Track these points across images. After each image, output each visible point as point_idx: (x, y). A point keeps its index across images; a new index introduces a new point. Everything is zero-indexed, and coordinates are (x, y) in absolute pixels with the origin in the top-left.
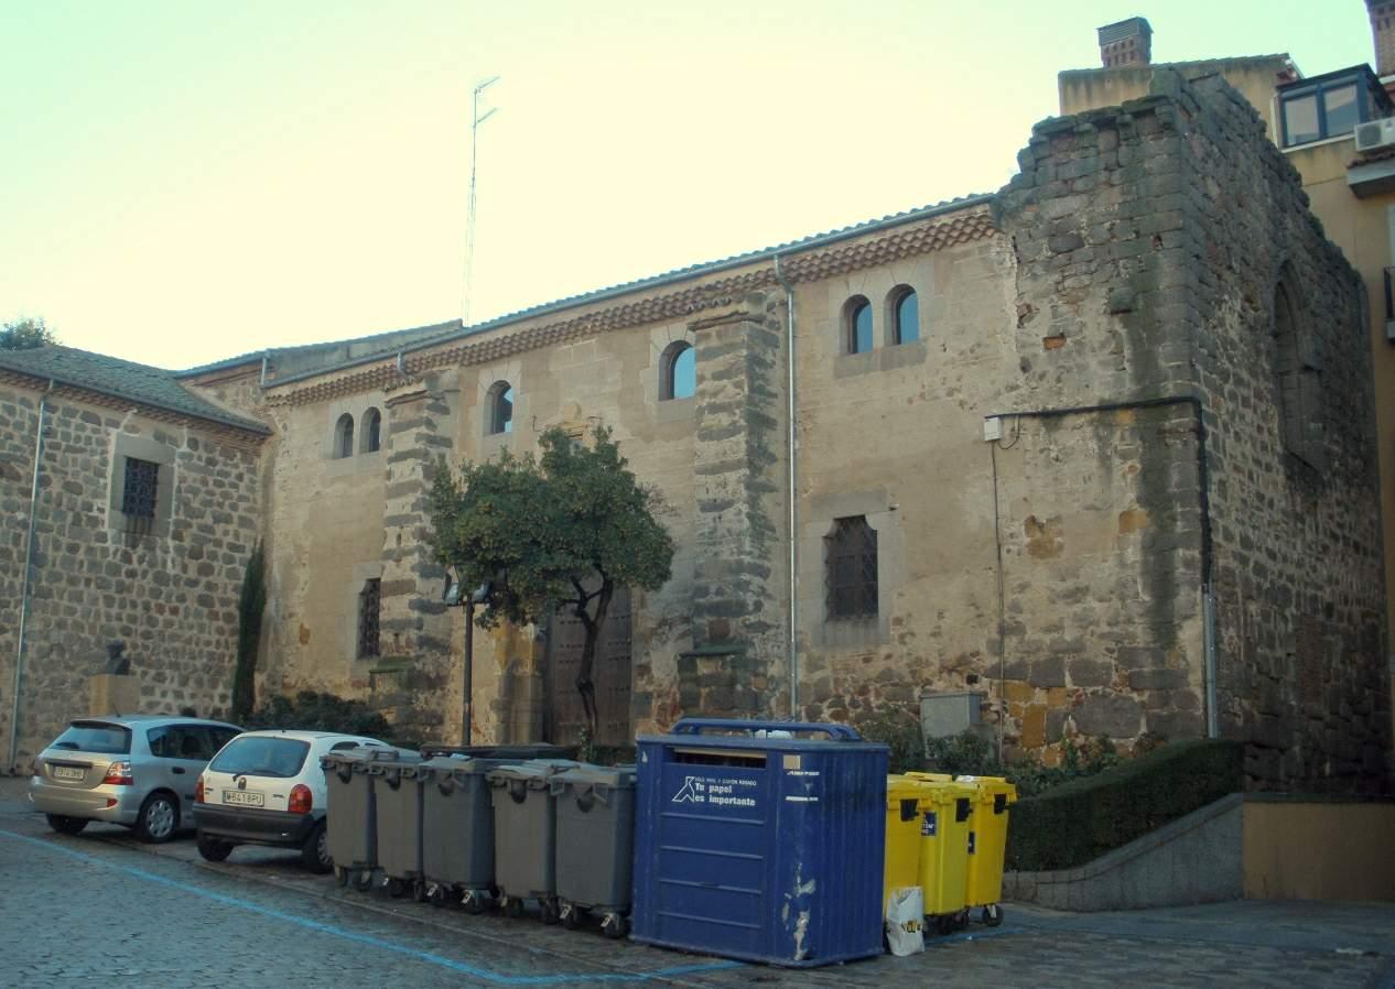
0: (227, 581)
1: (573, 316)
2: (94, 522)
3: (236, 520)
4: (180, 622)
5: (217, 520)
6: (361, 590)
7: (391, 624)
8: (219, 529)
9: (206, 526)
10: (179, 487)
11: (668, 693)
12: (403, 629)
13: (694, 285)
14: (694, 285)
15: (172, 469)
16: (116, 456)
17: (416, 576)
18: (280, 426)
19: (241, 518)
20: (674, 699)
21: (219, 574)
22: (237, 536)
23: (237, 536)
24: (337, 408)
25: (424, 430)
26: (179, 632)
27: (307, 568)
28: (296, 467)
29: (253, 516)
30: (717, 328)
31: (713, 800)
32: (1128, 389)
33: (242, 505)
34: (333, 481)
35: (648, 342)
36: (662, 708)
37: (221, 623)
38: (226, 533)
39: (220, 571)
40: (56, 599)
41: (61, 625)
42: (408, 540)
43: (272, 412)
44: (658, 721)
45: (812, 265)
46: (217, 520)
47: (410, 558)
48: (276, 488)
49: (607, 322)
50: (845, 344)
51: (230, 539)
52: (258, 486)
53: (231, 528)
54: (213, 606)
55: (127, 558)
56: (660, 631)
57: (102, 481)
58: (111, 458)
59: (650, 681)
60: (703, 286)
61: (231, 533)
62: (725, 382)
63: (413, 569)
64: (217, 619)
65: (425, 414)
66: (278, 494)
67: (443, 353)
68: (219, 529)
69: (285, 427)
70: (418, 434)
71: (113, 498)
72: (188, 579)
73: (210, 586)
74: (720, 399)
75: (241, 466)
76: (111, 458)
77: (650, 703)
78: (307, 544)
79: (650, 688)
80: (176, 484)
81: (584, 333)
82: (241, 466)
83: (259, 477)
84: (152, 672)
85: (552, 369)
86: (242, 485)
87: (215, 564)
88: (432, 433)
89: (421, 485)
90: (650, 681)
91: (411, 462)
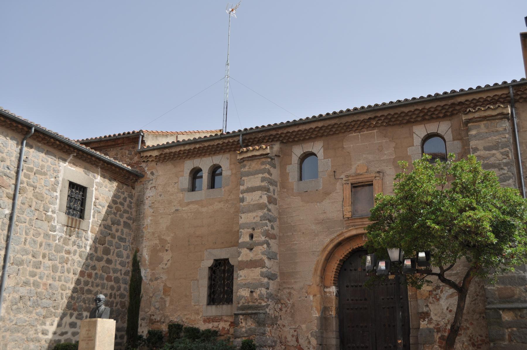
0: (117, 258)
2: (49, 219)
3: (122, 223)
4: (92, 282)
5: (113, 223)
6: (210, 266)
7: (246, 286)
8: (114, 228)
9: (108, 225)
10: (95, 202)
12: (257, 288)
13: (450, 102)
14: (450, 102)
15: (93, 191)
16: (63, 180)
17: (265, 258)
18: (149, 173)
19: (124, 222)
21: (113, 255)
22: (122, 233)
23: (122, 233)
24: (189, 165)
25: (266, 175)
26: (91, 288)
27: (169, 252)
28: (160, 195)
29: (130, 222)
30: (485, 122)
32: (66, 224)
33: (126, 215)
34: (188, 204)
35: (411, 134)
37: (112, 283)
38: (117, 231)
39: (113, 253)
40: (25, 266)
41: (26, 283)
42: (259, 236)
43: (143, 165)
45: (433, 114)
46: (113, 223)
47: (261, 247)
48: (146, 207)
49: (386, 121)
50: (190, 188)
51: (118, 234)
52: (133, 205)
53: (120, 228)
54: (110, 273)
55: (66, 242)
56: (434, 293)
57: (55, 194)
58: (60, 179)
60: (456, 102)
61: (120, 231)
62: (494, 152)
63: (263, 253)
64: (111, 281)
65: (268, 167)
66: (147, 210)
67: (271, 135)
68: (114, 228)
69: (152, 174)
70: (262, 178)
71: (61, 205)
72: (98, 256)
73: (109, 261)
74: (492, 160)
75: (126, 193)
76: (60, 179)
78: (168, 239)
79: (431, 326)
80: (94, 200)
81: (369, 126)
82: (126, 193)
83: (134, 201)
84: (76, 313)
85: (345, 146)
86: (126, 204)
87: (111, 248)
88: (271, 178)
89: (266, 206)
90: (430, 322)
91: (259, 193)
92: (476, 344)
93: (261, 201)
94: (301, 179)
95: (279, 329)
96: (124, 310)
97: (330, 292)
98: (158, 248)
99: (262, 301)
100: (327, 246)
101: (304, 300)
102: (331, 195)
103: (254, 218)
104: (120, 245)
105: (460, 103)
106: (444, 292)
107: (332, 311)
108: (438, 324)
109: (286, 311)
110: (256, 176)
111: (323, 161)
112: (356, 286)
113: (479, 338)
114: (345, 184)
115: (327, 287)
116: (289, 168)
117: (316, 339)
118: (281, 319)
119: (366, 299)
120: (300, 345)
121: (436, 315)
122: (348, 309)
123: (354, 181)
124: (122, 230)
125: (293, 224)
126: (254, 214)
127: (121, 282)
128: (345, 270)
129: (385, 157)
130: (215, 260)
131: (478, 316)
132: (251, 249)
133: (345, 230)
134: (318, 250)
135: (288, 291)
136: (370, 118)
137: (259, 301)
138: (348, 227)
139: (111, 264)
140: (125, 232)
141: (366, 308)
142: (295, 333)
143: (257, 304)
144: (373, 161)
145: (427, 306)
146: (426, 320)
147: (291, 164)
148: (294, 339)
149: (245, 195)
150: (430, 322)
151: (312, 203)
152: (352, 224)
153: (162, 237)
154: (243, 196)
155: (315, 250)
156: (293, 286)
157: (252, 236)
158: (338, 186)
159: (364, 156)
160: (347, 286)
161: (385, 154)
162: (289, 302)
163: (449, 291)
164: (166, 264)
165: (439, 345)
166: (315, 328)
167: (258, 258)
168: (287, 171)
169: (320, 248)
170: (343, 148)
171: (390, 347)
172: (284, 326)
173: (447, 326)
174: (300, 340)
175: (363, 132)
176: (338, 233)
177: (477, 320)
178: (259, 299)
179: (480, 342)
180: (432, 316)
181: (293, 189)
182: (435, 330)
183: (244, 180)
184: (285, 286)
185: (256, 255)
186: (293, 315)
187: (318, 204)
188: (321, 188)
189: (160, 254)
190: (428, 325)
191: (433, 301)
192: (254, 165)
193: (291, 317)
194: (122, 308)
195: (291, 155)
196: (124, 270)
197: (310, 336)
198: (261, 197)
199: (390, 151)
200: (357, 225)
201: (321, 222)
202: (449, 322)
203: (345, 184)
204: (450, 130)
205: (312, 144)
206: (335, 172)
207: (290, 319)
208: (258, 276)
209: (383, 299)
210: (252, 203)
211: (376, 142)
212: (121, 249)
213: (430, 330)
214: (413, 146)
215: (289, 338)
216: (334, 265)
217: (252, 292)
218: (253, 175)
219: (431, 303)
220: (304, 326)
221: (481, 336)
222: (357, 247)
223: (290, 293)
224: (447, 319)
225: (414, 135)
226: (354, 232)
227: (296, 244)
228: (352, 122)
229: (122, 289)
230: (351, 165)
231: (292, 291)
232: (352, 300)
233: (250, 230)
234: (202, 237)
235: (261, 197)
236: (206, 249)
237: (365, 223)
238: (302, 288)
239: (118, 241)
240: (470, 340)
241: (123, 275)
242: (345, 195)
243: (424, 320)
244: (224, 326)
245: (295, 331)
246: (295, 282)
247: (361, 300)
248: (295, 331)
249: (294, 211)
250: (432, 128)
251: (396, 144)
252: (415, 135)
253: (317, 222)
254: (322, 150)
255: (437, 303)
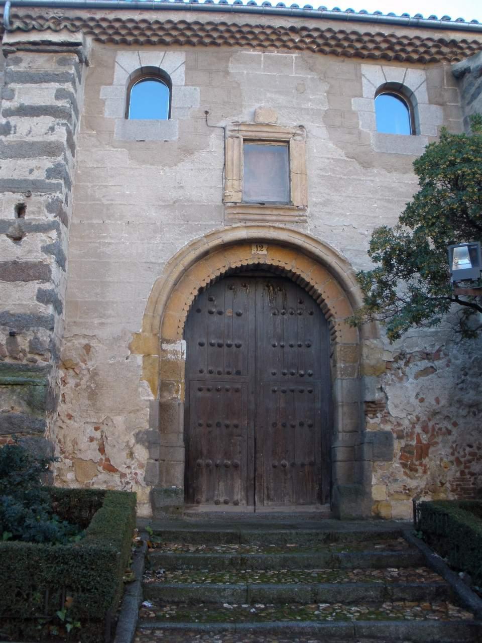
1: (287, 23)
11: (410, 435)
13: (437, 36)
14: (437, 36)
20: (419, 441)
31: (397, 570)
35: (359, 77)
36: (406, 450)
44: (404, 465)
47: (42, 236)
56: (395, 365)
59: (385, 420)
70: (58, 91)
77: (391, 445)
79: (388, 428)
85: (231, 71)
92: (462, 460)
93: (52, 138)
94: (126, 117)
95: (60, 423)
97: (175, 353)
99: (37, 357)
100: (182, 254)
101: (122, 364)
102: (196, 154)
103: (31, 171)
105: (453, 43)
106: (411, 365)
107: (177, 391)
108: (399, 424)
109: (77, 385)
110: (44, 85)
111: (183, 88)
112: (220, 346)
113: (468, 449)
114: (232, 137)
115: (168, 342)
116: (105, 92)
117: (149, 448)
118: (64, 401)
119: (238, 373)
120: (108, 460)
121: (396, 406)
122: (200, 390)
123: (250, 134)
125: (106, 202)
126: (32, 163)
128: (199, 311)
129: (309, 105)
131: (467, 410)
132: (17, 239)
133: (222, 227)
134: (161, 261)
135: (84, 342)
136: (293, 29)
137: (29, 356)
138: (232, 220)
141: (237, 391)
142: (98, 434)
143: (25, 362)
144: (286, 107)
145: (381, 389)
146: (379, 415)
147: (111, 84)
148: (95, 445)
149: (13, 120)
150: (385, 420)
151: (152, 164)
152: (241, 216)
154: (8, 123)
155: (153, 260)
156: (96, 332)
157: (20, 210)
158: (215, 141)
159: (269, 95)
160: (201, 345)
161: (310, 100)
162: (83, 366)
163: (419, 363)
165: (401, 463)
166: (146, 426)
167: (32, 258)
168: (102, 96)
169: (166, 258)
170: (227, 73)
171: (284, 466)
172: (70, 417)
173: (414, 427)
174: (108, 449)
175: (270, 52)
176: (208, 231)
177: (465, 417)
178: (30, 352)
179: (468, 457)
180: (390, 406)
181: (111, 133)
182: (395, 435)
183: (13, 90)
184: (76, 330)
185: (30, 252)
186: (93, 395)
187: (167, 169)
188: (175, 138)
190: (382, 426)
191: (392, 380)
192: (42, 63)
193: (89, 399)
195: (113, 67)
197: (133, 441)
198: (52, 129)
199: (318, 97)
200: (250, 220)
201: (173, 205)
202: (418, 419)
203: (232, 137)
204: (424, 85)
205: (162, 54)
206: (207, 112)
207: (87, 402)
208: (31, 299)
209: (274, 374)
210: (29, 139)
211: (294, 75)
213: (387, 436)
214: (361, 96)
215: (84, 443)
216: (187, 297)
217: (12, 335)
218: (36, 82)
219: (386, 383)
220: (119, 420)
221: (470, 446)
222: (239, 265)
223: (88, 348)
224: (415, 414)
225: (363, 79)
226: (243, 234)
227: (110, 244)
228: (257, 26)
230: (241, 106)
231: (93, 343)
232: (211, 372)
233: (19, 198)
235: (52, 129)
237: (268, 218)
238: (117, 339)
240: (453, 454)
242: (229, 158)
243: (375, 416)
245: (96, 429)
246: (102, 324)
247: (229, 373)
248: (96, 429)
249: (112, 177)
250: (395, 74)
251: (331, 87)
252: (364, 80)
253: (161, 203)
254: (183, 68)
255: (398, 385)
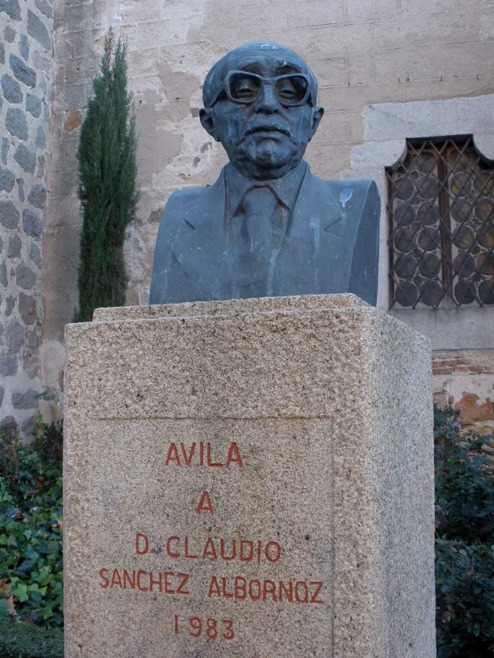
96: (31, 327)
98: (158, 107)
104: (17, 89)
124: (24, 39)
127: (21, 224)
130: (407, 140)
139: (10, 42)
140: (32, 49)
153: (176, 68)
164: (197, 160)
189: (170, 126)
194: (28, 322)
196: (30, 181)
212: (22, 106)
229: (24, 252)
234: (347, 61)
236: (370, 104)
239: (11, 73)
241: (26, 202)
244: (472, 389)
